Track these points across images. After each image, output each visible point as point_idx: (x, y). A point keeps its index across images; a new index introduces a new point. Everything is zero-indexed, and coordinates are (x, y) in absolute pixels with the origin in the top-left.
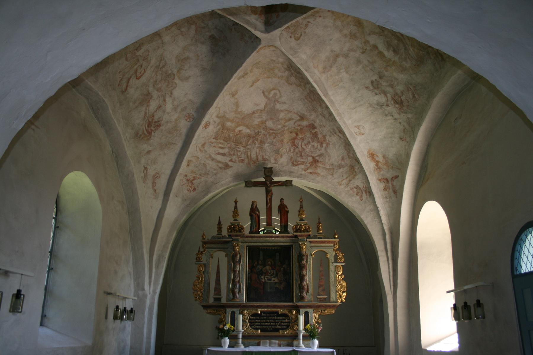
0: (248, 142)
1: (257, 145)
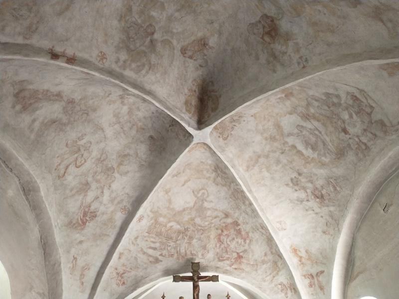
0: (178, 237)
1: (185, 241)
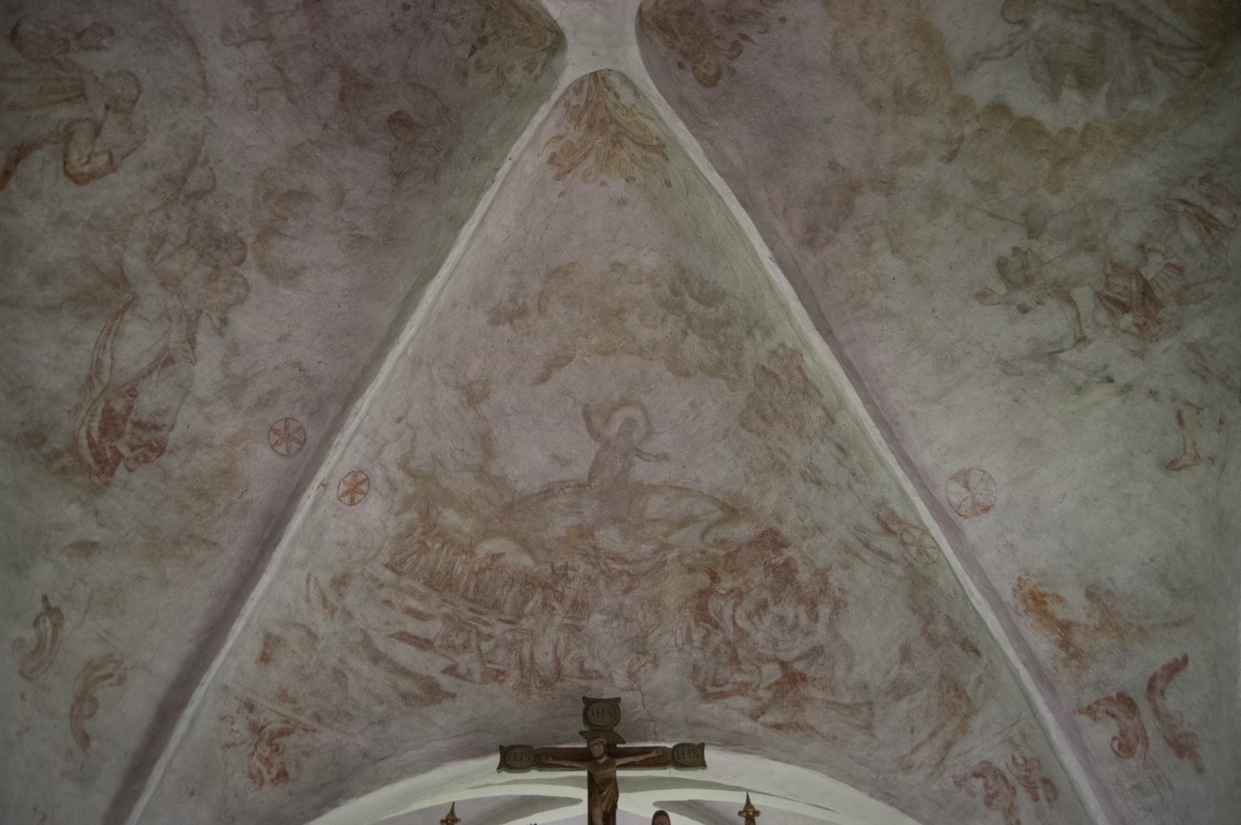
0: (525, 602)
1: (558, 620)
